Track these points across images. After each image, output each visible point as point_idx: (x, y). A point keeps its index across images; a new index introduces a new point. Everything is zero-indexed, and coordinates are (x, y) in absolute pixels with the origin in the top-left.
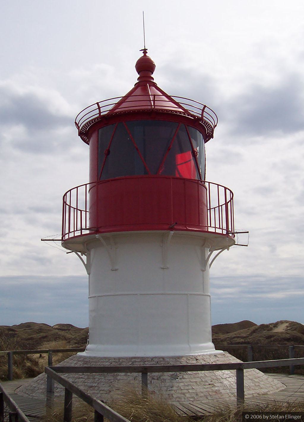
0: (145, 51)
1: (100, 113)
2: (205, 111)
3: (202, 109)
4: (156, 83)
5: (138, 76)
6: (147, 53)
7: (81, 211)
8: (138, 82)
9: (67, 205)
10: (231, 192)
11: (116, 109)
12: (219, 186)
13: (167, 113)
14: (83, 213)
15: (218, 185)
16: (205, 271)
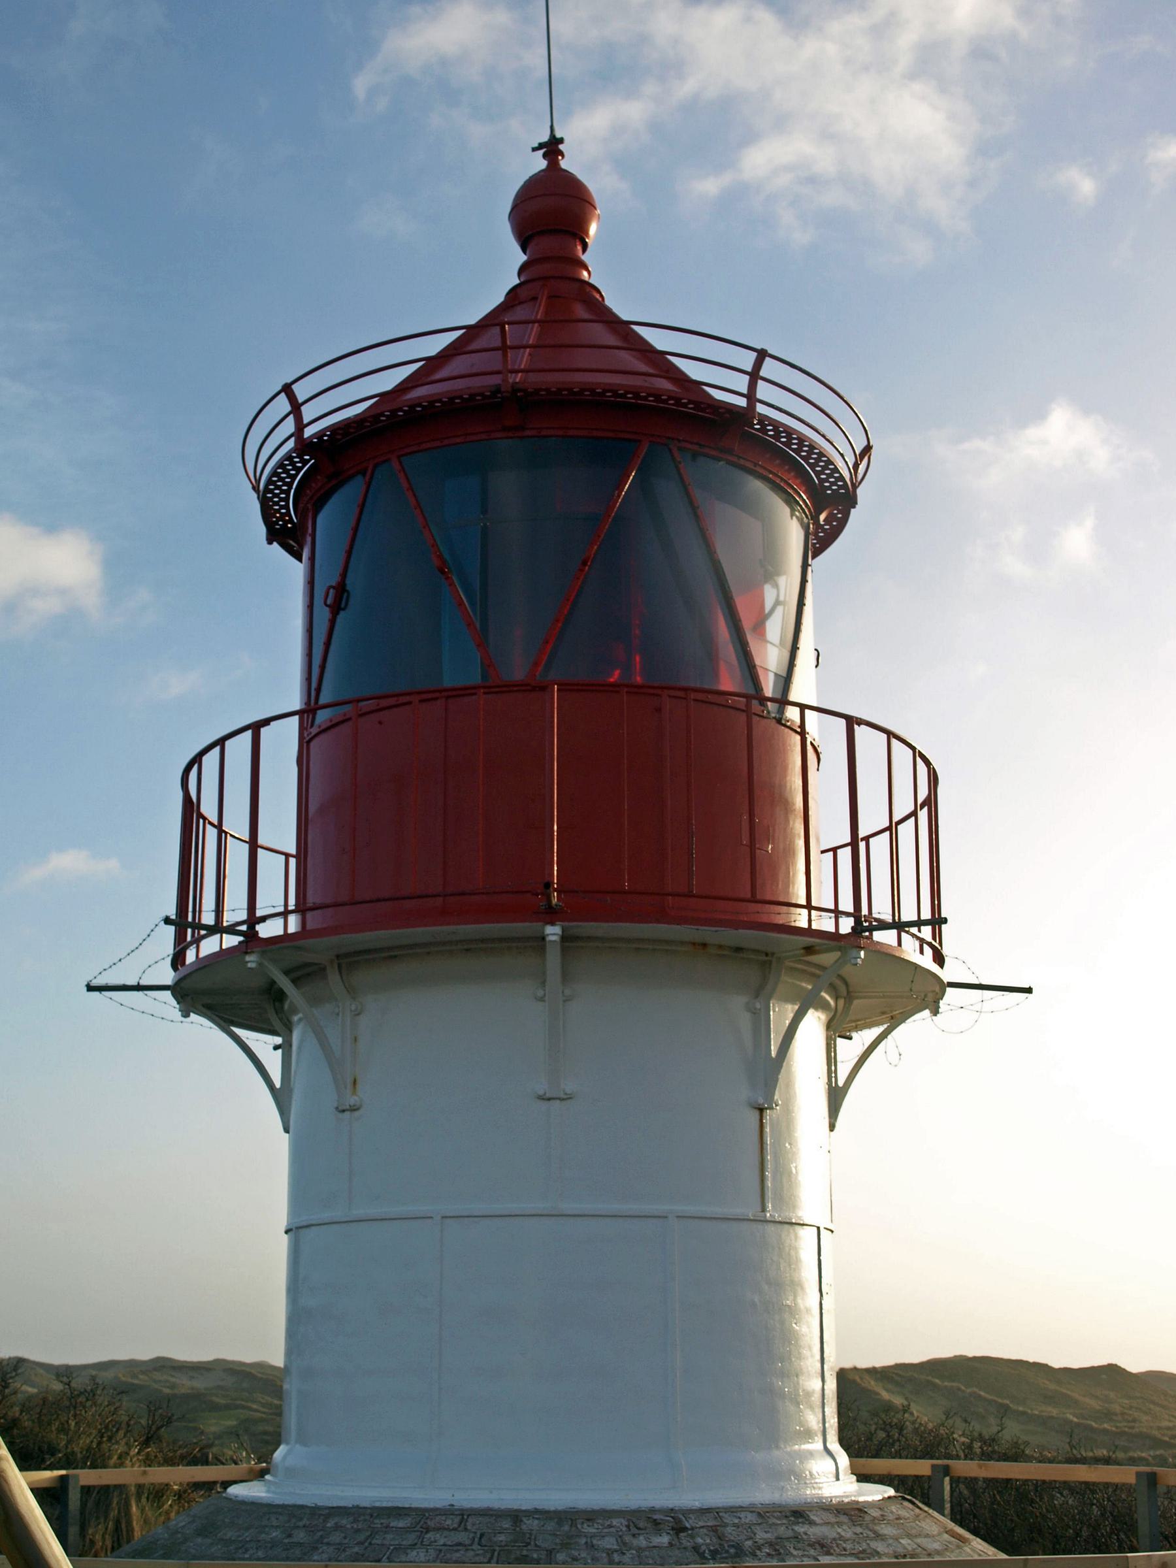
0: (552, 148)
1: (300, 426)
3: (749, 369)
4: (598, 291)
5: (523, 258)
8: (517, 281)
10: (918, 755)
11: (417, 386)
15: (890, 734)
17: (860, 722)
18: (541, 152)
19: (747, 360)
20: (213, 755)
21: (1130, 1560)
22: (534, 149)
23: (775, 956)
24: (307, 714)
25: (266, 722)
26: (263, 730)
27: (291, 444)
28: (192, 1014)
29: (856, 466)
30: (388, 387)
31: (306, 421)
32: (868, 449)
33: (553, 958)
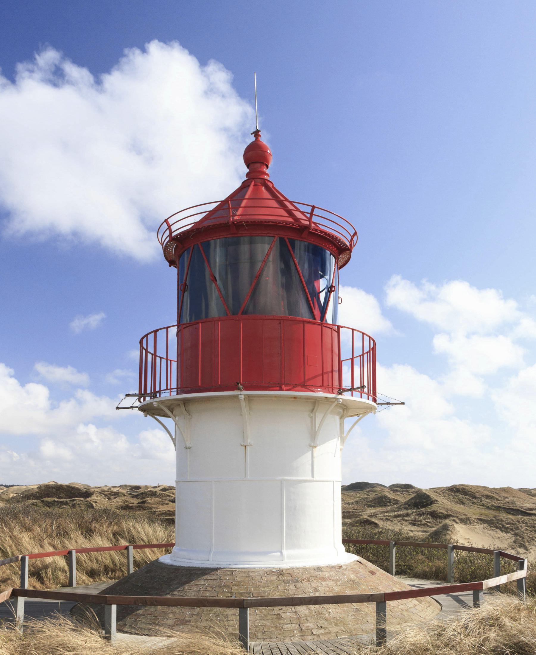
1: (171, 233)
2: (314, 213)
3: (310, 212)
5: (248, 170)
6: (260, 136)
7: (161, 358)
8: (246, 179)
9: (143, 350)
10: (374, 341)
12: (365, 336)
13: (293, 227)
14: (164, 362)
15: (353, 330)
16: (315, 447)
17: (342, 327)
18: (253, 135)
19: (309, 210)
21: (108, 599)
22: (252, 134)
23: (317, 400)
24: (178, 325)
25: (158, 330)
26: (157, 333)
27: (168, 239)
28: (148, 416)
29: (352, 239)
30: (211, 209)
31: (173, 231)
32: (356, 233)
33: (243, 404)
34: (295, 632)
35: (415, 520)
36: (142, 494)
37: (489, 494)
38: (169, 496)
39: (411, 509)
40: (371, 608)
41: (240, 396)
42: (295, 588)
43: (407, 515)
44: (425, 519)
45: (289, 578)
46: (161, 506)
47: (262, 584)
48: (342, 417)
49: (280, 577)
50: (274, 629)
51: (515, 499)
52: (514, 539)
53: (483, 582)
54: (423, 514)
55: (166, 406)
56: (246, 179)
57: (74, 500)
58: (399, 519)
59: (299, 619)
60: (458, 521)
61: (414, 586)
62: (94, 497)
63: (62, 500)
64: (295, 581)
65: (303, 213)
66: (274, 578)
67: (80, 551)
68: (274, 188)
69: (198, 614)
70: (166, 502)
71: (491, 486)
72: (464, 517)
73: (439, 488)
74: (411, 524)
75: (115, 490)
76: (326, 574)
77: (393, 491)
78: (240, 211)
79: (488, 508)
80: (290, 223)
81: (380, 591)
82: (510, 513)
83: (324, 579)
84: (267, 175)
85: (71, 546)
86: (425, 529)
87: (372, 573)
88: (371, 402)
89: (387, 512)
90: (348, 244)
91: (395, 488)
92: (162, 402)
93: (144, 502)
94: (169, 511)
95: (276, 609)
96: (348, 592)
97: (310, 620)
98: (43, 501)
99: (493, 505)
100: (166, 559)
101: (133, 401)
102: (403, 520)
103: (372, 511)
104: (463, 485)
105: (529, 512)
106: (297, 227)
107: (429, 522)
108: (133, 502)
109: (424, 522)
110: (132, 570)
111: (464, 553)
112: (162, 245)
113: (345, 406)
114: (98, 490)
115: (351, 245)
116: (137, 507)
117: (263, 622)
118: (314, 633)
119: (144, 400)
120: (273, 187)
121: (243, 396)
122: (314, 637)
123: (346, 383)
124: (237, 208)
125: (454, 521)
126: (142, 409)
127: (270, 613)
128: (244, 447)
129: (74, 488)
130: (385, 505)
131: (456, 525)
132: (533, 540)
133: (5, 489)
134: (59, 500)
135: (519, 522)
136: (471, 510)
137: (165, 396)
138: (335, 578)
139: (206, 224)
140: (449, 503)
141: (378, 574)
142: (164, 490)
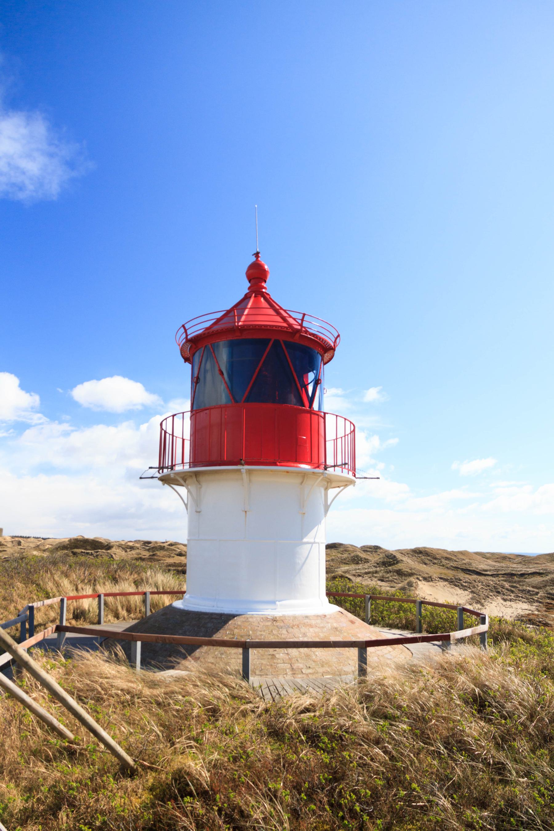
0: (257, 255)
1: (187, 335)
10: (354, 425)
14: (171, 436)
15: (337, 416)
19: (300, 316)
20: (165, 421)
24: (192, 411)
25: (175, 415)
27: (184, 340)
32: (339, 336)
34: (288, 670)
35: (383, 577)
36: (153, 548)
37: (448, 556)
38: (175, 551)
39: (379, 567)
40: (354, 652)
41: (242, 470)
42: (286, 633)
43: (376, 572)
44: (391, 576)
45: (282, 624)
46: (168, 559)
47: (259, 629)
48: (326, 489)
49: (274, 622)
50: (269, 667)
51: (471, 561)
52: (471, 596)
53: (451, 634)
54: (390, 572)
55: (181, 477)
56: (247, 291)
57: (97, 552)
58: (370, 575)
59: (290, 659)
60: (421, 579)
61: (401, 635)
62: (113, 550)
63: (88, 551)
64: (288, 627)
65: (294, 319)
66: (269, 623)
67: (106, 595)
68: (271, 299)
69: (206, 653)
70: (172, 555)
71: (450, 549)
72: (426, 575)
73: (404, 550)
74: (379, 580)
75: (131, 544)
76: (313, 622)
77: (364, 551)
78: (243, 318)
79: (447, 568)
80: (285, 327)
81: (359, 638)
82: (467, 574)
83: (311, 626)
84: (265, 288)
85: (101, 590)
86: (392, 585)
87: (352, 622)
88: (350, 476)
89: (359, 569)
90: (332, 345)
91: (367, 549)
92: (178, 474)
93: (154, 555)
94: (175, 563)
95: (271, 651)
96: (333, 639)
97: (300, 661)
98: (72, 552)
99: (452, 566)
100: (178, 604)
101: (154, 472)
102: (373, 576)
103: (345, 568)
104: (425, 548)
105: (484, 573)
106: (290, 330)
107: (396, 579)
108: (144, 554)
109: (391, 578)
110: (149, 613)
111: (430, 607)
112: (179, 345)
113: (329, 479)
114: (117, 544)
115: (334, 345)
116: (149, 559)
117: (260, 661)
118: (304, 672)
119: (163, 472)
120: (270, 298)
121: (245, 471)
122: (304, 676)
123: (330, 461)
124: (240, 316)
125: (418, 578)
126: (161, 479)
127: (266, 653)
128: (244, 513)
129: (97, 542)
130: (358, 563)
131: (419, 583)
132: (488, 597)
133: (43, 541)
134: (86, 551)
135: (475, 581)
136: (432, 570)
137: (178, 468)
138: (321, 625)
139: (216, 328)
140: (413, 563)
141: (357, 624)
142: (171, 545)
